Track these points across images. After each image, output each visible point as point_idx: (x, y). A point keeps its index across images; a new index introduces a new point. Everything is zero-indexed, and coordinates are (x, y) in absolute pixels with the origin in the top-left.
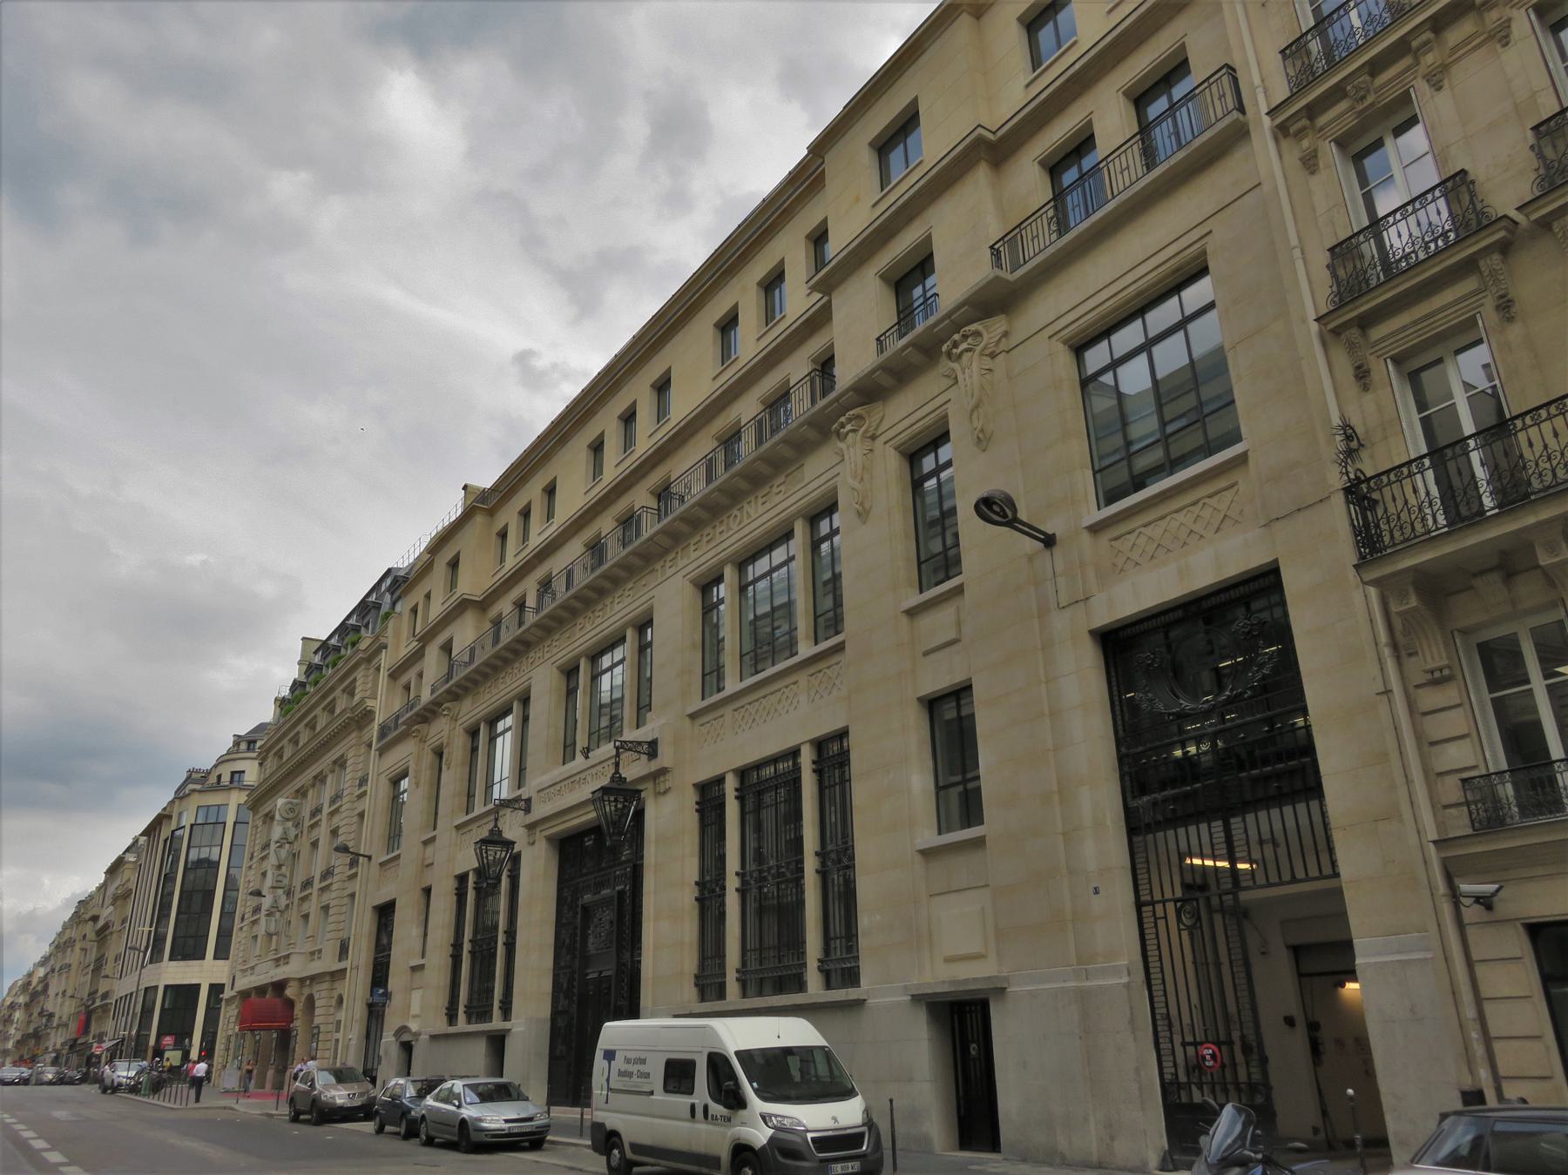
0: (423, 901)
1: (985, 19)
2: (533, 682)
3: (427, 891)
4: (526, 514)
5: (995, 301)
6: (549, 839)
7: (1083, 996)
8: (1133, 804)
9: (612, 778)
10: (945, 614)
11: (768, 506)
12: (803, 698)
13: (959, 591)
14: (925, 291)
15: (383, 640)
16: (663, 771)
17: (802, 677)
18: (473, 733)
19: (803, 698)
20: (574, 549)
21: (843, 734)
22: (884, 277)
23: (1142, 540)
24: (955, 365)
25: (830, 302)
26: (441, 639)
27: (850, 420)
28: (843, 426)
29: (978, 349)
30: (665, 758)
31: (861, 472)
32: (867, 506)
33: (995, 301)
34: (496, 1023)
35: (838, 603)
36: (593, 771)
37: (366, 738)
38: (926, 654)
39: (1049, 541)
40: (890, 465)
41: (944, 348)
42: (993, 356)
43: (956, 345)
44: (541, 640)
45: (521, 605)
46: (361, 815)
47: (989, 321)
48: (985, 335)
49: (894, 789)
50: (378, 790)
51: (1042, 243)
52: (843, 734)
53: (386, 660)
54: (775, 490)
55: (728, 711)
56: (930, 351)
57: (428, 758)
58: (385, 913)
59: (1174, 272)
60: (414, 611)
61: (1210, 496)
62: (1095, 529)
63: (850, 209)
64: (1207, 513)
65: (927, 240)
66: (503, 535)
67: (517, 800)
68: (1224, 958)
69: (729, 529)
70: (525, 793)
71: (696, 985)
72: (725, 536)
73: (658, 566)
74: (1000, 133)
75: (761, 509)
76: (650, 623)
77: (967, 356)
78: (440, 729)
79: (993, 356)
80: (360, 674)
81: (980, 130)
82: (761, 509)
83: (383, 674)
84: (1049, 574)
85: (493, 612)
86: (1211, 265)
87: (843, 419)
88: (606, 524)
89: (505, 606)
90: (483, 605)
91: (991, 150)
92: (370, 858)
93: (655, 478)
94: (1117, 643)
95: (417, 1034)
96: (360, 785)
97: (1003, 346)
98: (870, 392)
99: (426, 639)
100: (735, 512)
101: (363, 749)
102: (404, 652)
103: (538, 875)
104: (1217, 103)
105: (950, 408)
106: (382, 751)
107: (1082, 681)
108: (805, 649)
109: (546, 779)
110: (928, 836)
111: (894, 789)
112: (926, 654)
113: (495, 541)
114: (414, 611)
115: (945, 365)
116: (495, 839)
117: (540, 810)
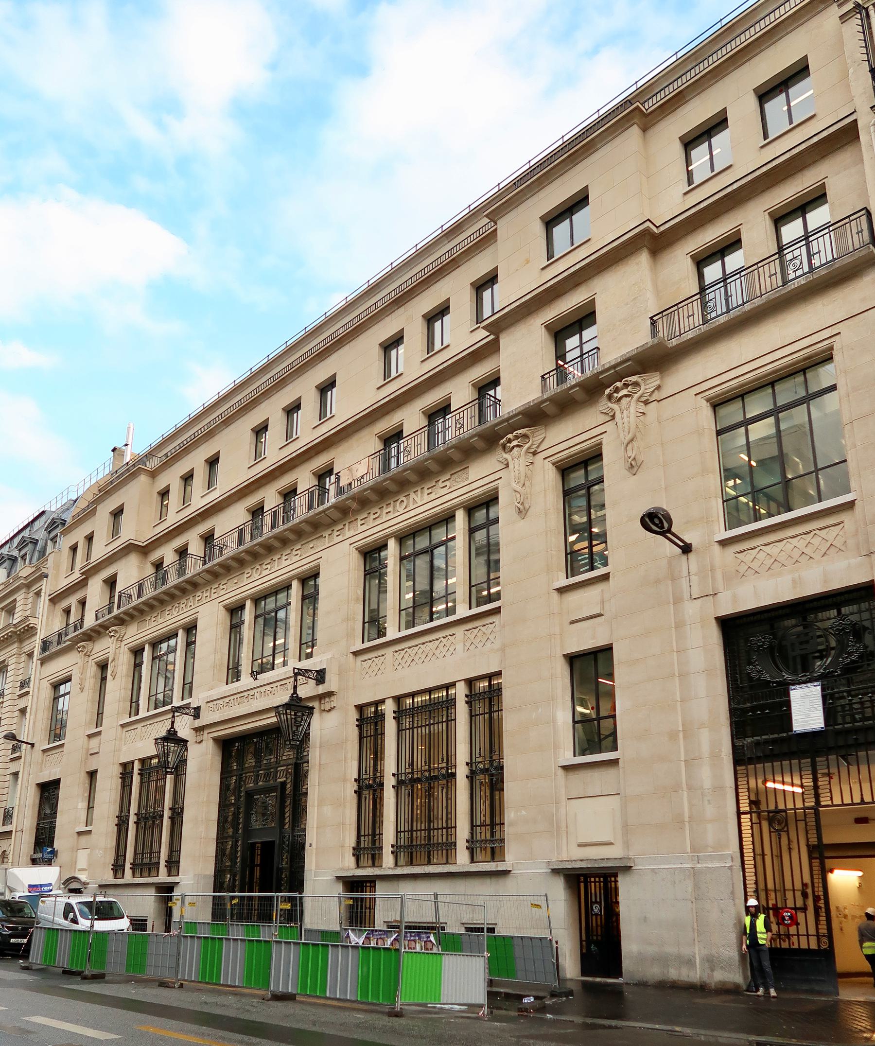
0: (87, 782)
1: (651, 132)
2: (199, 616)
3: (92, 775)
4: (188, 478)
5: (655, 360)
6: (216, 740)
7: (695, 873)
8: (739, 743)
9: (292, 697)
10: (593, 593)
11: (433, 496)
12: (459, 647)
13: (99, 733)
14: (581, 344)
15: (44, 570)
16: (330, 694)
17: (459, 631)
18: (137, 652)
19: (459, 647)
22: (548, 327)
23: (762, 555)
24: (615, 406)
25: (496, 341)
26: (106, 573)
27: (516, 437)
28: (510, 441)
29: (636, 396)
30: (331, 683)
31: (524, 481)
32: (527, 506)
33: (655, 360)
34: (163, 877)
36: (262, 689)
37: (27, 649)
38: (572, 622)
39: (686, 549)
40: (547, 479)
41: (607, 391)
42: (646, 403)
43: (617, 390)
44: (208, 583)
45: (182, 552)
46: (23, 711)
48: (643, 387)
49: (540, 722)
50: (41, 692)
51: (690, 324)
53: (48, 587)
54: (441, 484)
55: (389, 652)
57: (92, 670)
58: (49, 791)
59: (805, 359)
60: (74, 549)
62: (724, 543)
63: (522, 265)
64: (816, 541)
66: (164, 494)
67: (187, 706)
68: (767, 851)
69: (395, 511)
70: (194, 702)
71: (354, 855)
72: (391, 516)
74: (662, 229)
75: (427, 498)
76: (316, 575)
77: (625, 401)
78: (105, 647)
79: (646, 403)
80: (20, 597)
81: (648, 224)
82: (427, 498)
83: (44, 599)
84: (685, 573)
85: (155, 556)
86: (835, 358)
87: (510, 436)
88: (271, 498)
89: (168, 554)
90: (144, 550)
91: (654, 241)
92: (33, 745)
93: (319, 462)
94: (733, 628)
95: (85, 884)
96: (22, 686)
97: (656, 396)
98: (535, 417)
99: (88, 574)
101: (24, 657)
102: (64, 583)
103: (202, 765)
104: (855, 236)
105: (605, 439)
106: (43, 661)
107: (707, 654)
108: (462, 611)
109: (215, 693)
110: (568, 757)
111: (540, 722)
112: (572, 622)
113: (156, 498)
114: (74, 549)
115: (604, 404)
116: (171, 737)
117: (207, 718)
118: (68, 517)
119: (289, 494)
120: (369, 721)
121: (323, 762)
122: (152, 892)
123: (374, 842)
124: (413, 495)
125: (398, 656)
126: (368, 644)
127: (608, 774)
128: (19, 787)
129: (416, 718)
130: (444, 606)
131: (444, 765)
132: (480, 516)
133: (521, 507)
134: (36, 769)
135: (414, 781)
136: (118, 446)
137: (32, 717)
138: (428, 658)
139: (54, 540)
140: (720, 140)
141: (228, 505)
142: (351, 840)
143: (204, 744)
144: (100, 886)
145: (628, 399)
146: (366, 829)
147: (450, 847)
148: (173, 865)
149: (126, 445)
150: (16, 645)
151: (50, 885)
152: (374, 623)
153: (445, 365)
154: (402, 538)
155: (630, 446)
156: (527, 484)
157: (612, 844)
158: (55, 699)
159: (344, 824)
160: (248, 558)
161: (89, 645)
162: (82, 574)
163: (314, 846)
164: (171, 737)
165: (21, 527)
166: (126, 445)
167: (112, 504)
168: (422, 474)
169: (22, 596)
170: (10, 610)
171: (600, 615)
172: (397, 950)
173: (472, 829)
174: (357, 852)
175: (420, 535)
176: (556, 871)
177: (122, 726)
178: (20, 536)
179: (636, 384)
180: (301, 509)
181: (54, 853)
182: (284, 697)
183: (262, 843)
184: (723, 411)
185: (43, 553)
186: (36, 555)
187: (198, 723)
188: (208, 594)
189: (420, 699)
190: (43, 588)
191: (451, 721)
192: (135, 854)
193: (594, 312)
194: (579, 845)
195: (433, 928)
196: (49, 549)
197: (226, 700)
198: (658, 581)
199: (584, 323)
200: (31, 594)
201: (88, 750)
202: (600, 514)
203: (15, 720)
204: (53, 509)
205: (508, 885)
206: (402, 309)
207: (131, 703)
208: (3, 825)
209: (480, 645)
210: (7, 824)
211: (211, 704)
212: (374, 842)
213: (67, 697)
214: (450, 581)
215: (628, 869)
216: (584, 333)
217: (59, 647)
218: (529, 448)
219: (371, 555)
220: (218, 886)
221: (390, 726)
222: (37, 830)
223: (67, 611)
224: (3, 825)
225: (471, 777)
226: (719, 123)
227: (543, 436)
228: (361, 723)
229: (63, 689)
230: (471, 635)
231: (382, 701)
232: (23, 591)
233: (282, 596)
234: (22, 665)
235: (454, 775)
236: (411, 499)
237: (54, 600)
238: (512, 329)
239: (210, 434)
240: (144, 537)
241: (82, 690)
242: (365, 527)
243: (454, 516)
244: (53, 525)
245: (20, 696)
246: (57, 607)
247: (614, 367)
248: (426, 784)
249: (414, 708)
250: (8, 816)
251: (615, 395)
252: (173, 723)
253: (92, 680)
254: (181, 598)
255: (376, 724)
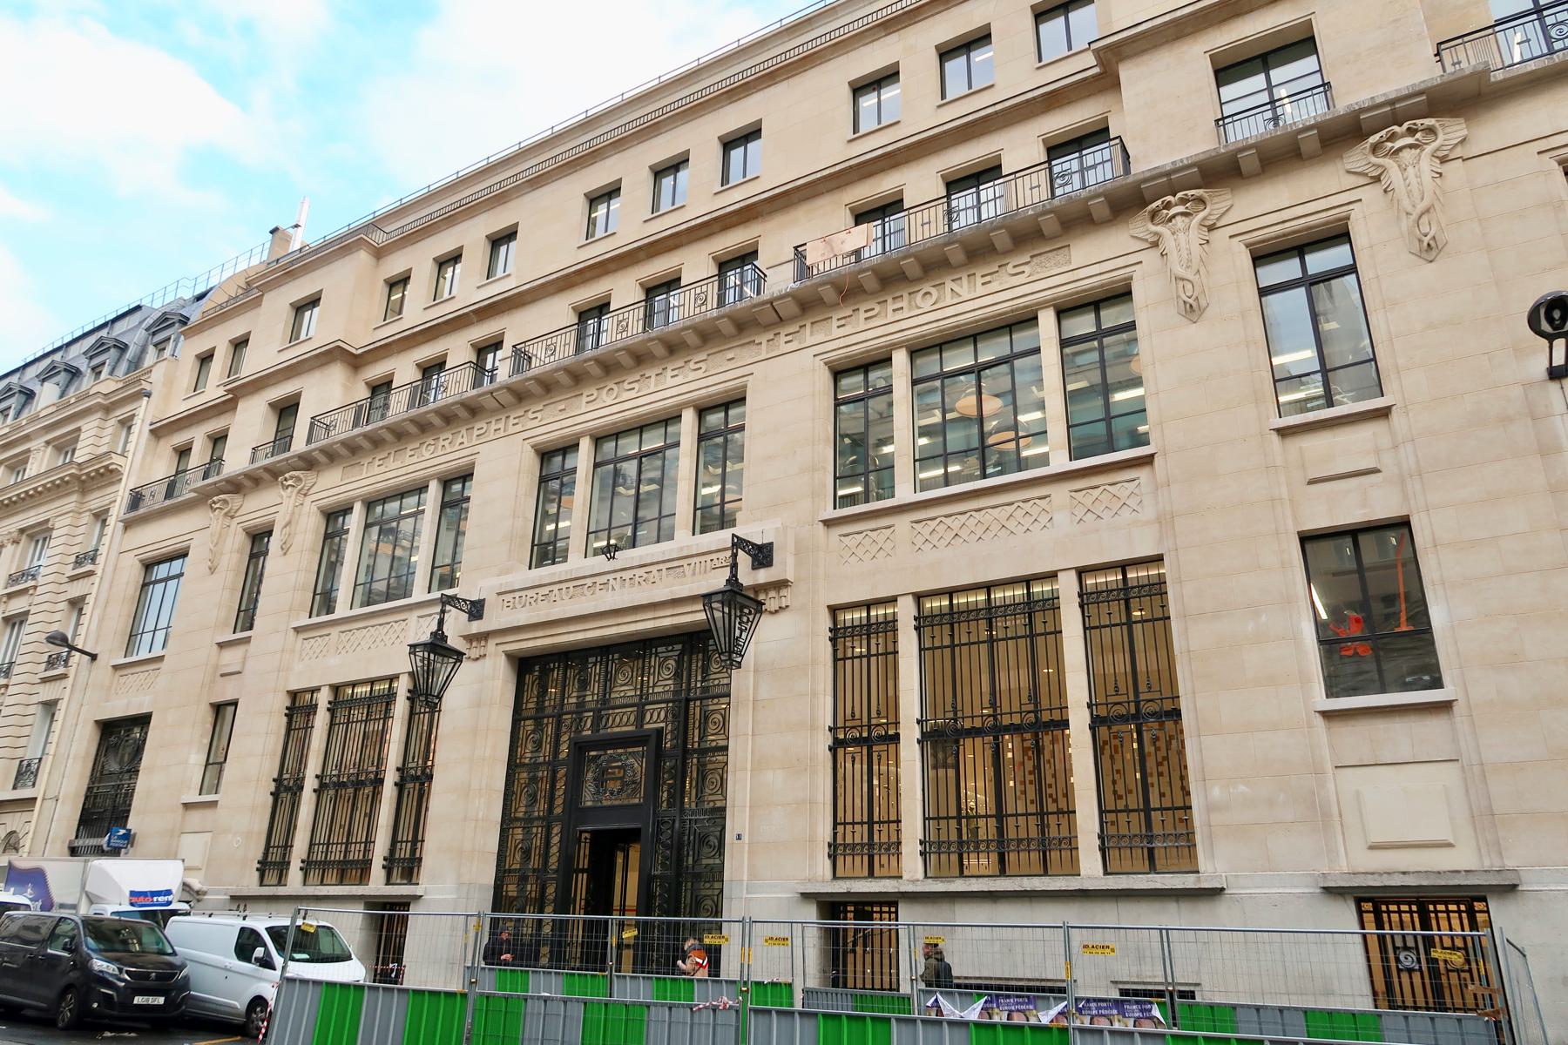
0: (210, 719)
2: (479, 460)
3: (222, 711)
6: (510, 656)
12: (1061, 518)
13: (247, 640)
15: (145, 385)
16: (781, 585)
20: (558, 312)
21: (143, 720)
22: (272, 405)
27: (1183, 201)
32: (1203, 303)
34: (377, 884)
35: (255, 608)
36: (627, 575)
38: (1312, 482)
41: (1374, 139)
47: (1446, 121)
48: (1441, 137)
52: (143, 720)
53: (146, 414)
54: (692, 365)
55: (334, 631)
56: (274, 473)
57: (236, 544)
60: (206, 359)
61: (1025, 501)
65: (298, 395)
72: (899, 316)
73: (365, 461)
77: (1407, 155)
80: (89, 426)
83: (141, 429)
85: (376, 371)
90: (356, 362)
96: (79, 562)
97: (1458, 152)
98: (235, 486)
100: (926, 287)
101: (86, 518)
106: (128, 525)
108: (1060, 462)
118: (195, 314)
119: (432, 369)
120: (858, 635)
121: (764, 693)
122: (360, 908)
123: (413, 851)
124: (949, 285)
125: (925, 529)
126: (315, 620)
127: (1433, 726)
128: (57, 726)
129: (873, 642)
130: (942, 471)
131: (1031, 707)
132: (715, 419)
133: (1195, 305)
134: (93, 697)
135: (340, 785)
136: (282, 226)
137: (96, 613)
138: (990, 534)
139: (160, 346)
140: (889, 93)
141: (534, 301)
142: (824, 831)
143: (487, 662)
144: (233, 898)
145: (1415, 152)
146: (277, 839)
147: (364, 868)
148: (405, 865)
149: (297, 226)
150: (74, 497)
151: (168, 892)
152: (325, 600)
153: (998, 107)
154: (917, 350)
155: (1425, 219)
156: (1202, 270)
157: (1450, 845)
158: (145, 585)
159: (812, 802)
160: (322, 458)
161: (235, 500)
162: (229, 391)
163: (746, 838)
164: (437, 646)
165: (78, 333)
166: (297, 226)
167: (300, 289)
168: (1027, 235)
169: (96, 423)
170: (17, 465)
171: (1376, 471)
172: (1064, 1030)
173: (835, 828)
174: (264, 867)
175: (1021, 330)
176: (1332, 892)
177: (297, 630)
178: (47, 362)
179: (1431, 131)
180: (398, 405)
181: (129, 838)
182: (719, 581)
183: (591, 832)
184: (846, 382)
185: (136, 363)
186: (124, 366)
187: (476, 627)
188: (501, 425)
189: (881, 612)
190: (141, 412)
191: (387, 716)
192: (394, 841)
193: (298, 404)
194: (1372, 848)
195: (1160, 994)
196: (151, 357)
197: (545, 590)
198: (1506, 420)
199: (1271, 59)
200: (113, 422)
201: (217, 667)
202: (738, 466)
203: (58, 616)
204: (156, 306)
205: (1220, 914)
206: (894, 37)
207: (315, 594)
208: (15, 788)
209: (1106, 515)
210: (24, 786)
211: (508, 597)
212: (413, 851)
213: (172, 584)
214: (561, 525)
215: (1511, 889)
216: (1272, 73)
217: (168, 502)
218: (1205, 219)
219: (553, 455)
220: (500, 901)
221: (321, 719)
222: (87, 797)
223: (183, 452)
224: (15, 788)
225: (400, 786)
226: (888, 76)
227: (1229, 203)
228: (291, 712)
229: (162, 571)
230: (1087, 499)
231: (318, 689)
232: (99, 415)
233: (411, 501)
234: (82, 530)
235: (382, 781)
236: (948, 291)
237: (158, 433)
238: (1146, 57)
239: (500, 199)
240: (359, 341)
241: (212, 570)
242: (842, 332)
243: (1036, 318)
244: (165, 321)
245: (73, 579)
246: (162, 442)
247: (1392, 102)
248: (351, 788)
249: (869, 625)
250: (26, 773)
251: (1389, 144)
252: (441, 622)
253: (235, 556)
254: (441, 430)
255: (388, 704)
